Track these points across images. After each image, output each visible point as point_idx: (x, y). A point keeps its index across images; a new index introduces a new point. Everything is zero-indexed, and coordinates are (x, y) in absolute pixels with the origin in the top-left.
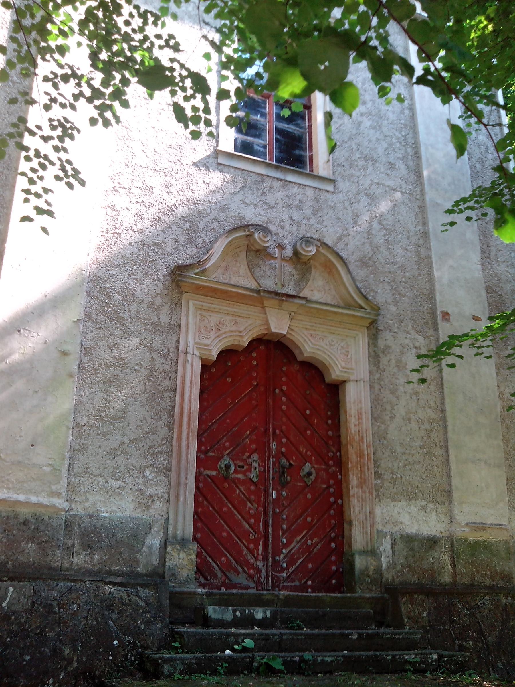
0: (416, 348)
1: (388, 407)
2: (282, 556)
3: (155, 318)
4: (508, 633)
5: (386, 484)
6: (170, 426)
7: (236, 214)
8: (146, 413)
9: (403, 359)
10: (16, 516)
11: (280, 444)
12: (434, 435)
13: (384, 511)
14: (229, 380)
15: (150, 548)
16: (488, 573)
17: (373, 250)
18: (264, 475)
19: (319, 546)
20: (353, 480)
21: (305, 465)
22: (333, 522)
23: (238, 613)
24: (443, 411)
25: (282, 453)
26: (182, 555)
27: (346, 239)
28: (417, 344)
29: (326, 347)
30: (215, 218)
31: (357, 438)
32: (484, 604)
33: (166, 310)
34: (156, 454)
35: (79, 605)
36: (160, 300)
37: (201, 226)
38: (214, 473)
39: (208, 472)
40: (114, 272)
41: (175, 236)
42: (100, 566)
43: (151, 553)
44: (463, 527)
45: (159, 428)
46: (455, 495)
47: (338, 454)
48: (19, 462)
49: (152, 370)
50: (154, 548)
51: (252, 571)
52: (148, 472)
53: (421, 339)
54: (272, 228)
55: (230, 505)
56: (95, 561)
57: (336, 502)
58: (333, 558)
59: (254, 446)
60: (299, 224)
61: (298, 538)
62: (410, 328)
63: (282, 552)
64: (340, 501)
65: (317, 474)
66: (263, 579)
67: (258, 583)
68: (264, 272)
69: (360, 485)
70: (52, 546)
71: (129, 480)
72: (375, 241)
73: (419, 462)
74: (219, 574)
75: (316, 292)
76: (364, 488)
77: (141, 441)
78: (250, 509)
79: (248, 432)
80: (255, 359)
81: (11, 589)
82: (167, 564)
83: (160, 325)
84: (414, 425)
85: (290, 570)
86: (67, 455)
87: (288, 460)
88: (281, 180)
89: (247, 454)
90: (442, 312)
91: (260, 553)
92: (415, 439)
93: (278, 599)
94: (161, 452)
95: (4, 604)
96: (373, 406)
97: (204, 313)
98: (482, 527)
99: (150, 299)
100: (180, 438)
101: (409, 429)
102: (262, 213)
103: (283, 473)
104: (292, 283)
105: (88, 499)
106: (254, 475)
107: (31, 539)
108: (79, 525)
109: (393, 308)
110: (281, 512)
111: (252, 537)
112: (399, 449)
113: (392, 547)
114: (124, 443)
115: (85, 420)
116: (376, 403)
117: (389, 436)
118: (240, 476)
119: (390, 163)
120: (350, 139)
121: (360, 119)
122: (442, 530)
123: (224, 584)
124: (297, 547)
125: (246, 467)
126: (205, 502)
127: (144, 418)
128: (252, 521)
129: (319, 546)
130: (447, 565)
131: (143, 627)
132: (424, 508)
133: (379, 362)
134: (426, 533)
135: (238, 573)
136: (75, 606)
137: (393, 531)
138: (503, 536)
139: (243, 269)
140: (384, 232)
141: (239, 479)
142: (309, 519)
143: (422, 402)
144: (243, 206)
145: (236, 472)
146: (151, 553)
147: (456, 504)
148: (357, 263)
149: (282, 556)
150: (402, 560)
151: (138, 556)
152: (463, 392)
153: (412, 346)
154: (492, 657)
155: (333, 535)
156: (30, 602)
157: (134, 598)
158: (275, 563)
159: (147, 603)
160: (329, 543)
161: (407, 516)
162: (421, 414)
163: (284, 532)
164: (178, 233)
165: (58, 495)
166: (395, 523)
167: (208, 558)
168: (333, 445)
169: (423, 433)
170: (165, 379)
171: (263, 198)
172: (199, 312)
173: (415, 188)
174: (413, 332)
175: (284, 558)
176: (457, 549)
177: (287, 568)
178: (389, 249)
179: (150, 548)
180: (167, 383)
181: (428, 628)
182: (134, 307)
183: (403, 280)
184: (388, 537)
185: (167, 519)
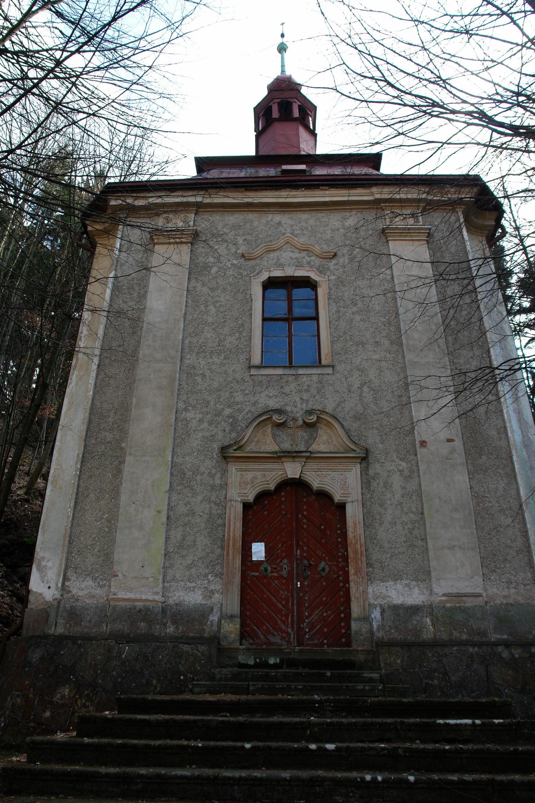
0: (400, 471)
1: (378, 517)
2: (305, 624)
3: (212, 482)
4: (471, 674)
5: (376, 571)
6: (222, 548)
7: (263, 405)
8: (207, 541)
9: (389, 481)
10: (135, 608)
11: (302, 551)
12: (416, 532)
13: (375, 589)
14: (266, 513)
15: (212, 622)
16: (465, 630)
17: (363, 407)
18: (290, 572)
19: (332, 617)
20: (352, 571)
21: (321, 563)
22: (342, 599)
23: (258, 660)
24: (422, 513)
25: (304, 556)
26: (230, 626)
27: (343, 405)
28: (401, 468)
29: (329, 482)
30: (250, 411)
31: (353, 541)
32: (451, 653)
33: (218, 475)
34: (215, 565)
35: (163, 656)
36: (215, 470)
37: (240, 419)
38: (257, 574)
39: (254, 574)
40: (187, 458)
41: (223, 428)
42: (182, 634)
43: (212, 625)
44: (440, 596)
45: (216, 549)
46: (433, 574)
47: (346, 553)
48: (136, 577)
49: (211, 514)
50: (214, 622)
51: (284, 635)
52: (210, 576)
53: (404, 464)
54: (288, 408)
55: (268, 593)
56: (180, 631)
57: (344, 586)
58: (343, 624)
59: (284, 554)
60: (307, 401)
61: (317, 612)
62: (395, 457)
63: (305, 622)
64: (347, 585)
65: (330, 568)
66: (292, 640)
67: (289, 643)
68: (283, 439)
69: (356, 573)
70: (155, 623)
71: (199, 582)
72: (365, 400)
73: (404, 553)
74: (262, 637)
75: (321, 445)
76: (359, 575)
77: (205, 558)
78: (282, 595)
79: (280, 545)
80: (284, 496)
81: (127, 648)
82: (221, 631)
83: (215, 486)
84: (399, 527)
85: (311, 633)
86: (162, 571)
87: (308, 561)
88: (294, 375)
89: (279, 560)
90: (420, 442)
91: (290, 623)
92: (400, 537)
93: (294, 651)
94: (217, 564)
95: (123, 656)
96: (365, 517)
97: (243, 473)
98: (459, 596)
99: (209, 471)
100: (228, 554)
101: (395, 530)
102: (281, 400)
103: (305, 570)
104: (303, 442)
105: (175, 595)
106: (284, 573)
107: (143, 620)
108: (170, 611)
109: (381, 446)
110: (304, 595)
111: (284, 613)
112: (386, 545)
113: (381, 615)
114: (195, 560)
115: (172, 550)
116: (368, 515)
117: (378, 537)
118: (275, 574)
119: (376, 342)
120: (345, 333)
121: (352, 317)
122: (424, 600)
123: (265, 644)
124: (316, 618)
125: (279, 568)
126: (252, 593)
127: (207, 545)
128: (284, 602)
129: (332, 617)
130: (429, 625)
131: (199, 668)
132: (408, 585)
133: (370, 486)
134: (410, 603)
135: (274, 635)
136: (161, 656)
137: (383, 603)
138: (479, 601)
139: (269, 439)
140: (372, 392)
141: (274, 576)
142: (324, 599)
143: (405, 509)
144: (268, 399)
145: (272, 572)
146: (212, 625)
147: (434, 580)
148: (351, 419)
149: (305, 624)
150: (390, 623)
151: (205, 627)
152: (439, 498)
153: (396, 470)
154: (453, 691)
155: (342, 609)
156: (136, 655)
157: (195, 651)
158: (300, 629)
159: (203, 655)
160: (340, 614)
161: (393, 591)
162: (404, 518)
163: (307, 608)
164: (226, 426)
165: (157, 593)
166: (384, 598)
167: (255, 627)
168: (342, 548)
169: (406, 531)
170: (219, 519)
171: (282, 390)
172: (239, 473)
173: (397, 355)
174: (397, 460)
175: (307, 625)
176: (436, 614)
177: (309, 632)
178: (377, 404)
179: (212, 622)
180: (220, 521)
181: (401, 671)
182: (199, 478)
183: (389, 424)
184: (378, 608)
185: (222, 604)
